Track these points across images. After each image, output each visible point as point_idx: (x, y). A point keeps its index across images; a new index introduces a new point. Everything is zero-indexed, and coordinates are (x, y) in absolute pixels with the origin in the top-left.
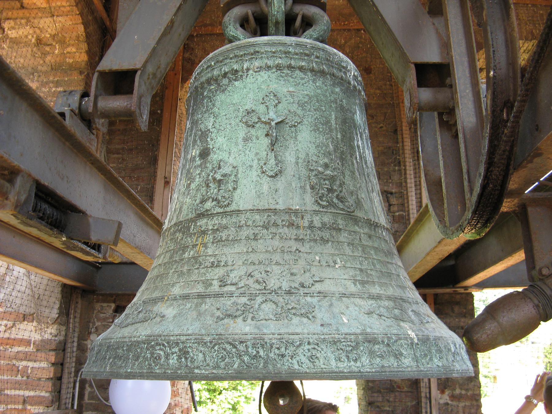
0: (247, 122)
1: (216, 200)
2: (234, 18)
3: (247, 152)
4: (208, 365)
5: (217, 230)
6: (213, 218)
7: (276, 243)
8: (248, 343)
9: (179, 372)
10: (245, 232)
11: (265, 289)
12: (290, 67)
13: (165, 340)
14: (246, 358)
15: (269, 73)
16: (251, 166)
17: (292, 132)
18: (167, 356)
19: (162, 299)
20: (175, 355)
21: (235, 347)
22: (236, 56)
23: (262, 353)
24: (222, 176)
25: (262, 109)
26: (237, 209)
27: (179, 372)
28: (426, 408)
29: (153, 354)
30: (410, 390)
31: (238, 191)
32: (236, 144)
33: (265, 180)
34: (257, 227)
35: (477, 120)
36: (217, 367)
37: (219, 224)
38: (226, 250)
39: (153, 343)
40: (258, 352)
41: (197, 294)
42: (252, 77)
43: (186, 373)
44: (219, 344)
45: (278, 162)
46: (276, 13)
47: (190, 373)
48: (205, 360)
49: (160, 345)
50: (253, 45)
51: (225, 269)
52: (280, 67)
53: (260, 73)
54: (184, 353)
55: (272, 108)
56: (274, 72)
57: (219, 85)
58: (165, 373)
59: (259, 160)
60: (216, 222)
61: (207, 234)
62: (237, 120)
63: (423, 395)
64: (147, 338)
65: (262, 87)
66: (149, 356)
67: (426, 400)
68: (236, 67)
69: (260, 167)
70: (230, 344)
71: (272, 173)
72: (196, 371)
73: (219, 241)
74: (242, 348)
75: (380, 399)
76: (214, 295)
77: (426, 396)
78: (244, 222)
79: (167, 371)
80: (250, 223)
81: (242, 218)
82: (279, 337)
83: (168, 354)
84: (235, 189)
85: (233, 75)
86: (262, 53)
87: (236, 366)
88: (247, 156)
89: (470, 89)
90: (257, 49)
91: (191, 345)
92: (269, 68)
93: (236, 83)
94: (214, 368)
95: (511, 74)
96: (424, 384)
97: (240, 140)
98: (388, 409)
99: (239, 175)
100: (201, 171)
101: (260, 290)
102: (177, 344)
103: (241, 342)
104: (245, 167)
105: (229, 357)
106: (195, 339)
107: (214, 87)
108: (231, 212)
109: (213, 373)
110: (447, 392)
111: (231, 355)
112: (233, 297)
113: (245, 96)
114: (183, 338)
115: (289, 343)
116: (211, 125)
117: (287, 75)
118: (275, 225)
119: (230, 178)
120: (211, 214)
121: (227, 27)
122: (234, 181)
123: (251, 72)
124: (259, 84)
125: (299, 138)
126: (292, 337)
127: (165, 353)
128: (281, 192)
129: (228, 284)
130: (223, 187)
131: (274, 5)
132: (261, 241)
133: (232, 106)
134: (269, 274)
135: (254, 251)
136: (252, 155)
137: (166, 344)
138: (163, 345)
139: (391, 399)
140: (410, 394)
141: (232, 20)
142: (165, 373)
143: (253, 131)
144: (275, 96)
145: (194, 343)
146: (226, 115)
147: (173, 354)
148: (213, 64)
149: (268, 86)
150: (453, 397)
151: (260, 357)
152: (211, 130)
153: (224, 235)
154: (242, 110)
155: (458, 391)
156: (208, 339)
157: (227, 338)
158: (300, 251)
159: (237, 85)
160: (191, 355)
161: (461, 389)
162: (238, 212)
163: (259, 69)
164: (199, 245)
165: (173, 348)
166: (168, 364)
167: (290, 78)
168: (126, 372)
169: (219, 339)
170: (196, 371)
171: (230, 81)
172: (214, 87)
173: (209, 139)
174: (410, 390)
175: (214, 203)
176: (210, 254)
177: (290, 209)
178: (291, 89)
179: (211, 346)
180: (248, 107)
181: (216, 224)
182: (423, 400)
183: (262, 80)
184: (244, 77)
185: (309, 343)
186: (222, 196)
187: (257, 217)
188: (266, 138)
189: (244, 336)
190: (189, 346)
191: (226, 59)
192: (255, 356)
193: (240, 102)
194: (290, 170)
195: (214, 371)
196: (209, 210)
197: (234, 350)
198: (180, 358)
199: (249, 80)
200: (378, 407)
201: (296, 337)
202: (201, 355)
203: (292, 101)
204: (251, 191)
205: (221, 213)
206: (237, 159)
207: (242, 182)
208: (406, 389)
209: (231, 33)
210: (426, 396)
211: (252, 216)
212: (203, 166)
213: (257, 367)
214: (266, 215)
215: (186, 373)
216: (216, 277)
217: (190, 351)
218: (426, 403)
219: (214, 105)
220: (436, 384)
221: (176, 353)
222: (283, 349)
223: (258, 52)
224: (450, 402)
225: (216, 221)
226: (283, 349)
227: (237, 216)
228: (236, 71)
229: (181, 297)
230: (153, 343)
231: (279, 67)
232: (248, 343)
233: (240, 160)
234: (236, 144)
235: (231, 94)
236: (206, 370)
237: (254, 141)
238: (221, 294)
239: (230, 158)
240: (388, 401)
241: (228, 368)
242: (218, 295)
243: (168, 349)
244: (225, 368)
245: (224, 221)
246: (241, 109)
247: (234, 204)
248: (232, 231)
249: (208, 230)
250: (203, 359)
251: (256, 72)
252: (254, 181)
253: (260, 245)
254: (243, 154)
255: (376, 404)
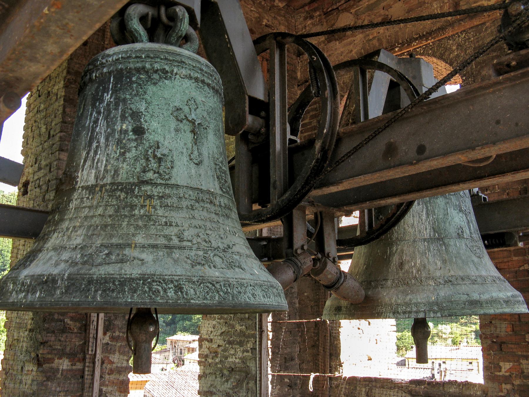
0: (177, 116)
1: (158, 173)
2: (138, 14)
3: (178, 140)
4: (199, 297)
5: (162, 197)
6: (156, 187)
7: (205, 214)
8: (221, 283)
9: (179, 302)
10: (185, 203)
11: (211, 247)
12: (203, 82)
13: (160, 278)
14: (221, 293)
15: (190, 82)
16: (182, 153)
17: (205, 133)
18: (165, 291)
19: (129, 245)
20: (172, 289)
21: (213, 285)
22: (166, 59)
23: (229, 290)
24: (162, 155)
25: (186, 109)
26: (176, 183)
27: (179, 302)
28: (92, 347)
29: (150, 289)
30: (79, 331)
31: (175, 170)
32: (169, 132)
33: (192, 166)
34: (192, 200)
35: (281, 147)
36: (205, 298)
37: (163, 192)
38: (173, 214)
39: (149, 280)
40: (227, 290)
41: (164, 245)
42: (179, 81)
43: (184, 302)
44: (204, 283)
45: (200, 154)
46: (183, 29)
47: (187, 302)
48: (196, 293)
49: (156, 282)
50: (180, 55)
51: (178, 228)
52: (198, 80)
53: (184, 80)
54: (179, 288)
55: (193, 110)
56: (193, 83)
57: (150, 77)
58: (167, 302)
59: (187, 149)
60: (160, 190)
61: (154, 199)
62: (169, 112)
63: (91, 336)
64: (142, 276)
65: (186, 92)
66: (147, 290)
67: (93, 340)
68: (167, 68)
69: (188, 155)
70: (211, 283)
71: (196, 162)
72: (192, 301)
73: (165, 206)
74: (218, 286)
75: (53, 339)
76: (178, 247)
77: (94, 336)
78: (183, 195)
79: (169, 301)
80: (186, 196)
81: (181, 192)
82: (236, 280)
83: (165, 289)
84: (172, 167)
85: (163, 73)
86: (186, 64)
87: (217, 298)
88: (178, 143)
89: (279, 125)
90: (183, 60)
91: (184, 283)
92: (190, 78)
93: (166, 81)
94: (204, 299)
95: (330, 133)
96: (94, 326)
97: (172, 129)
98: (59, 347)
99: (174, 157)
100: (137, 145)
101: (208, 247)
102: (172, 282)
103: (217, 283)
104: (178, 152)
105: (211, 292)
106: (186, 279)
107: (144, 77)
108: (172, 185)
109: (204, 303)
110: (108, 334)
111: (212, 291)
112: (192, 250)
113: (174, 95)
114: (176, 278)
115: (242, 285)
116: (144, 109)
117: (201, 87)
118: (203, 201)
119: (168, 158)
120: (155, 183)
121: (132, 20)
122: (172, 161)
123: (178, 76)
124: (184, 88)
125: (209, 138)
126: (243, 281)
127: (162, 288)
128: (202, 176)
129: (185, 240)
130: (163, 164)
131: (184, 23)
132: (196, 211)
133: (163, 99)
134: (209, 236)
135: (194, 218)
136: (182, 144)
137: (162, 282)
138: (160, 282)
139: (62, 339)
140: (79, 335)
141: (136, 15)
142: (167, 302)
143: (181, 125)
144: (195, 102)
145: (185, 282)
146: (158, 105)
147: (170, 289)
148: (143, 56)
149: (190, 92)
150: (112, 338)
151: (229, 292)
152: (144, 113)
153: (169, 201)
154: (172, 105)
155: (117, 333)
156: (195, 279)
157: (208, 280)
158: (219, 222)
159: (167, 83)
160: (185, 290)
161: (120, 332)
162: (177, 186)
163: (184, 77)
164: (148, 206)
165: (169, 284)
166: (168, 296)
167: (202, 91)
168: (126, 301)
169: (203, 279)
170: (192, 301)
171: (160, 78)
172: (144, 77)
173: (142, 120)
174: (79, 331)
175: (156, 175)
176: (160, 215)
177: (210, 191)
178: (203, 99)
179: (198, 284)
180: (177, 104)
181: (161, 192)
182: (91, 340)
183: (186, 86)
184: (173, 79)
185: (251, 286)
186: (163, 171)
187: (191, 193)
188: (190, 133)
189: (217, 279)
190: (183, 284)
191: (157, 57)
192: (226, 292)
193: (170, 99)
194: (206, 162)
195: (205, 301)
196: (153, 180)
197: (213, 288)
198: (176, 292)
199: (177, 82)
200: (50, 346)
201: (245, 281)
202: (192, 290)
203: (204, 109)
204: (184, 172)
205: (163, 184)
206: (171, 144)
207: (177, 163)
208: (76, 330)
209: (135, 26)
210: (94, 336)
211: (188, 191)
212: (139, 141)
213: (229, 300)
214: (196, 192)
215: (184, 302)
216: (173, 234)
217: (184, 287)
218: (93, 343)
219: (145, 93)
220: (102, 327)
221: (172, 288)
222: (239, 288)
223: (184, 62)
224: (109, 342)
225: (160, 189)
226: (239, 288)
227: (177, 189)
228: (167, 72)
229: (149, 246)
230: (149, 280)
231: (196, 80)
232: (221, 283)
233: (173, 146)
234: (169, 132)
235: (162, 89)
236: (199, 301)
237: (183, 133)
238: (184, 247)
239: (165, 142)
240: (60, 340)
241: (213, 300)
242: (181, 247)
243: (164, 285)
244: (211, 300)
245: (167, 191)
246: (171, 104)
247: (173, 179)
248: (175, 200)
249: (154, 195)
250: (194, 293)
251: (182, 78)
252: (186, 164)
253: (196, 213)
254: (175, 142)
255: (49, 343)
